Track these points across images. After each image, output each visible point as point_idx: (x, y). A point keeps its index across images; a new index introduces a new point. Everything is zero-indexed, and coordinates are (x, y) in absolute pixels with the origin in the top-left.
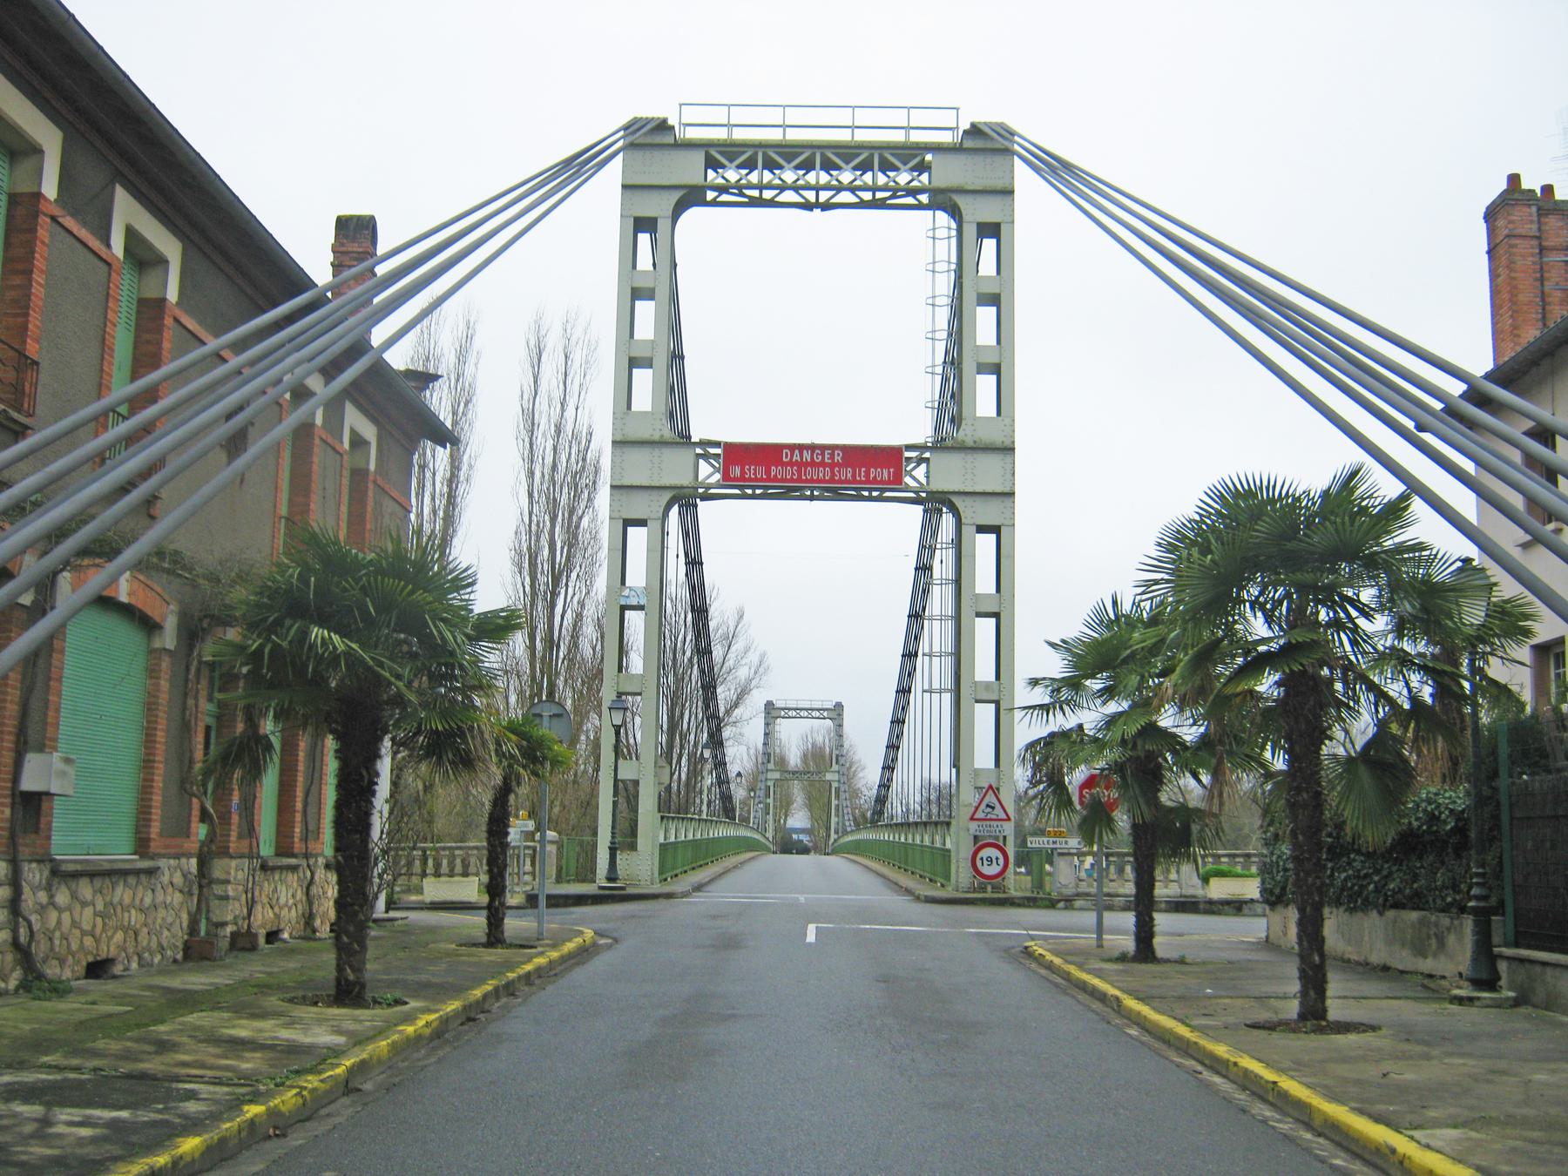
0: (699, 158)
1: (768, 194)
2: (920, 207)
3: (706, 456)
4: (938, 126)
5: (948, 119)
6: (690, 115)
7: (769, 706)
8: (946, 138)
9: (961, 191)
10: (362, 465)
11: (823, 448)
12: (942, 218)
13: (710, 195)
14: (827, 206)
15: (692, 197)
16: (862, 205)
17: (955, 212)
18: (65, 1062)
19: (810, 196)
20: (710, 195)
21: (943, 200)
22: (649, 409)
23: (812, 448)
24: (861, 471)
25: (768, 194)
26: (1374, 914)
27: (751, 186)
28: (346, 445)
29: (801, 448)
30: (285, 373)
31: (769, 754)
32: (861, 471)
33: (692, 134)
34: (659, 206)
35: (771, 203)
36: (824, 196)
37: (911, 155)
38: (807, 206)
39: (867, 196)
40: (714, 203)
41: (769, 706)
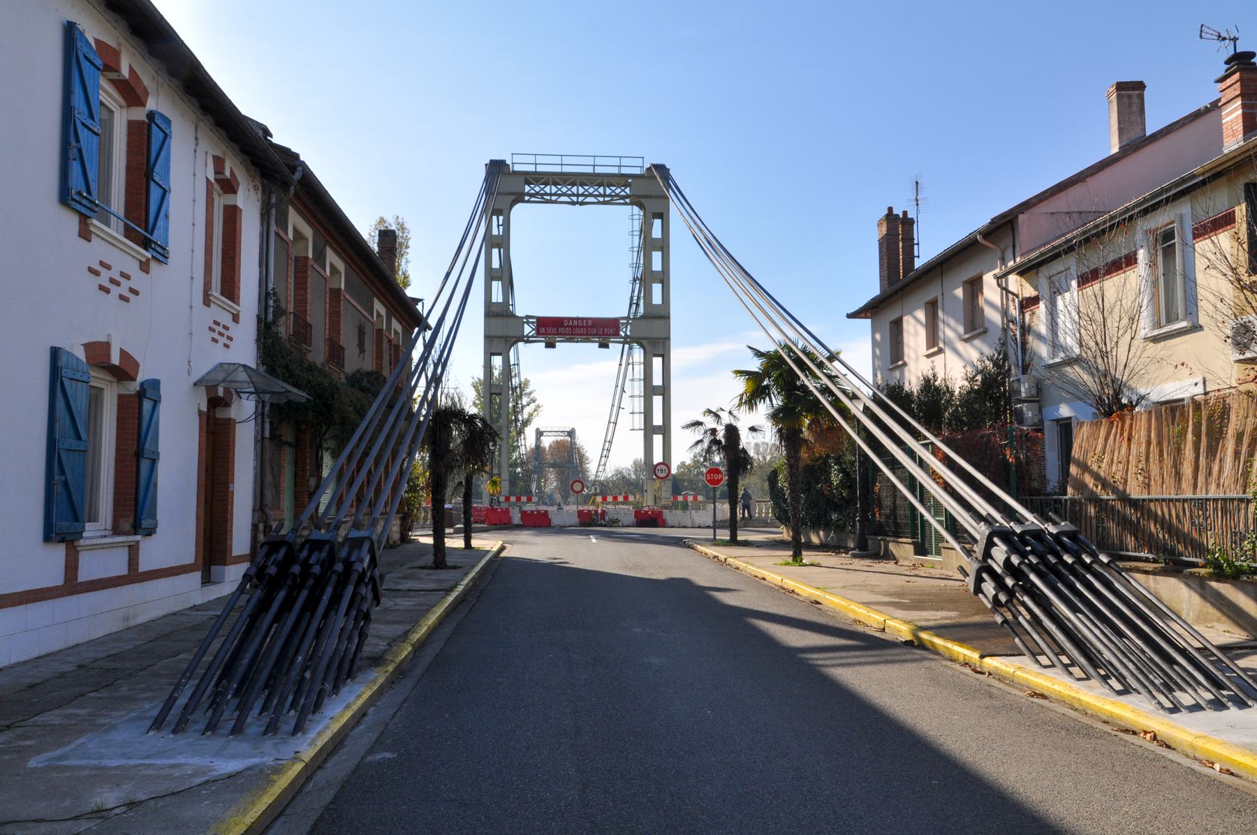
0: (522, 179)
1: (554, 198)
2: (626, 204)
3: (528, 323)
4: (633, 168)
5: (639, 162)
6: (517, 159)
7: (537, 430)
8: (637, 171)
9: (646, 197)
10: (302, 254)
11: (583, 319)
12: (636, 209)
13: (527, 198)
14: (582, 203)
15: (519, 198)
16: (599, 203)
17: (641, 206)
18: (172, 771)
19: (575, 199)
20: (527, 198)
21: (636, 200)
22: (869, 321)
23: (578, 319)
24: (598, 331)
25: (554, 198)
26: (688, 462)
27: (546, 194)
28: (291, 236)
29: (573, 319)
30: (1069, 657)
31: (538, 448)
32: (598, 331)
33: (517, 168)
34: (503, 202)
35: (555, 202)
36: (581, 199)
37: (621, 179)
38: (573, 203)
39: (601, 199)
40: (528, 201)
41: (537, 430)
